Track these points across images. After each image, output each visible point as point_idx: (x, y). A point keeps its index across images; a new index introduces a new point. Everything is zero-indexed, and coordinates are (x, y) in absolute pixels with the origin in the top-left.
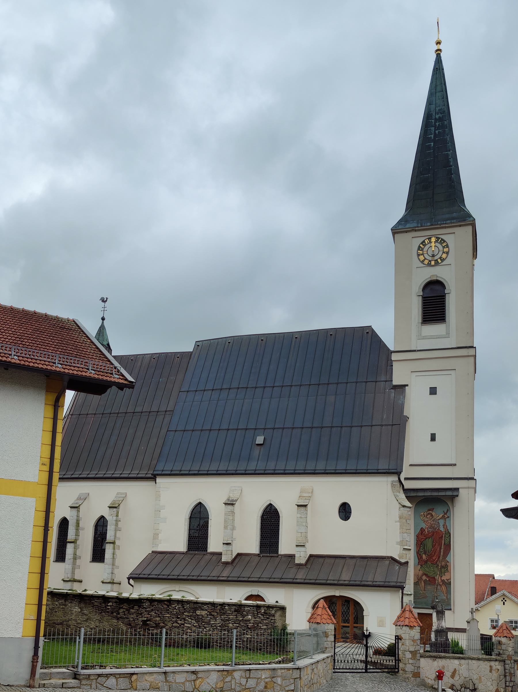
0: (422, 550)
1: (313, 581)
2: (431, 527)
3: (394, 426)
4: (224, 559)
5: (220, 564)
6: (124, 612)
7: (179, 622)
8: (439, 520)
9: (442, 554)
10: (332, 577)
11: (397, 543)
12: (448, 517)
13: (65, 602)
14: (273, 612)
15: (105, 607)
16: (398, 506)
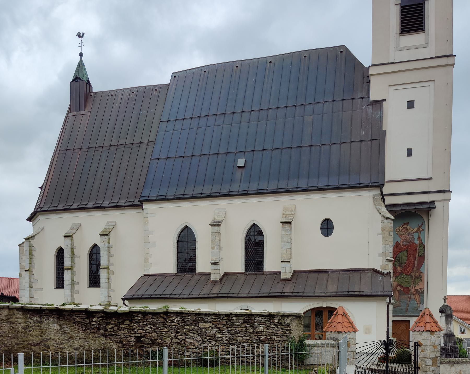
0: (397, 263)
1: (301, 294)
2: (406, 240)
3: (373, 141)
4: (212, 278)
5: (209, 282)
6: (112, 328)
7: (180, 337)
8: (414, 233)
9: (416, 265)
10: (319, 290)
11: (380, 255)
12: (423, 230)
13: (40, 318)
14: (288, 321)
15: (90, 323)
16: (380, 218)
